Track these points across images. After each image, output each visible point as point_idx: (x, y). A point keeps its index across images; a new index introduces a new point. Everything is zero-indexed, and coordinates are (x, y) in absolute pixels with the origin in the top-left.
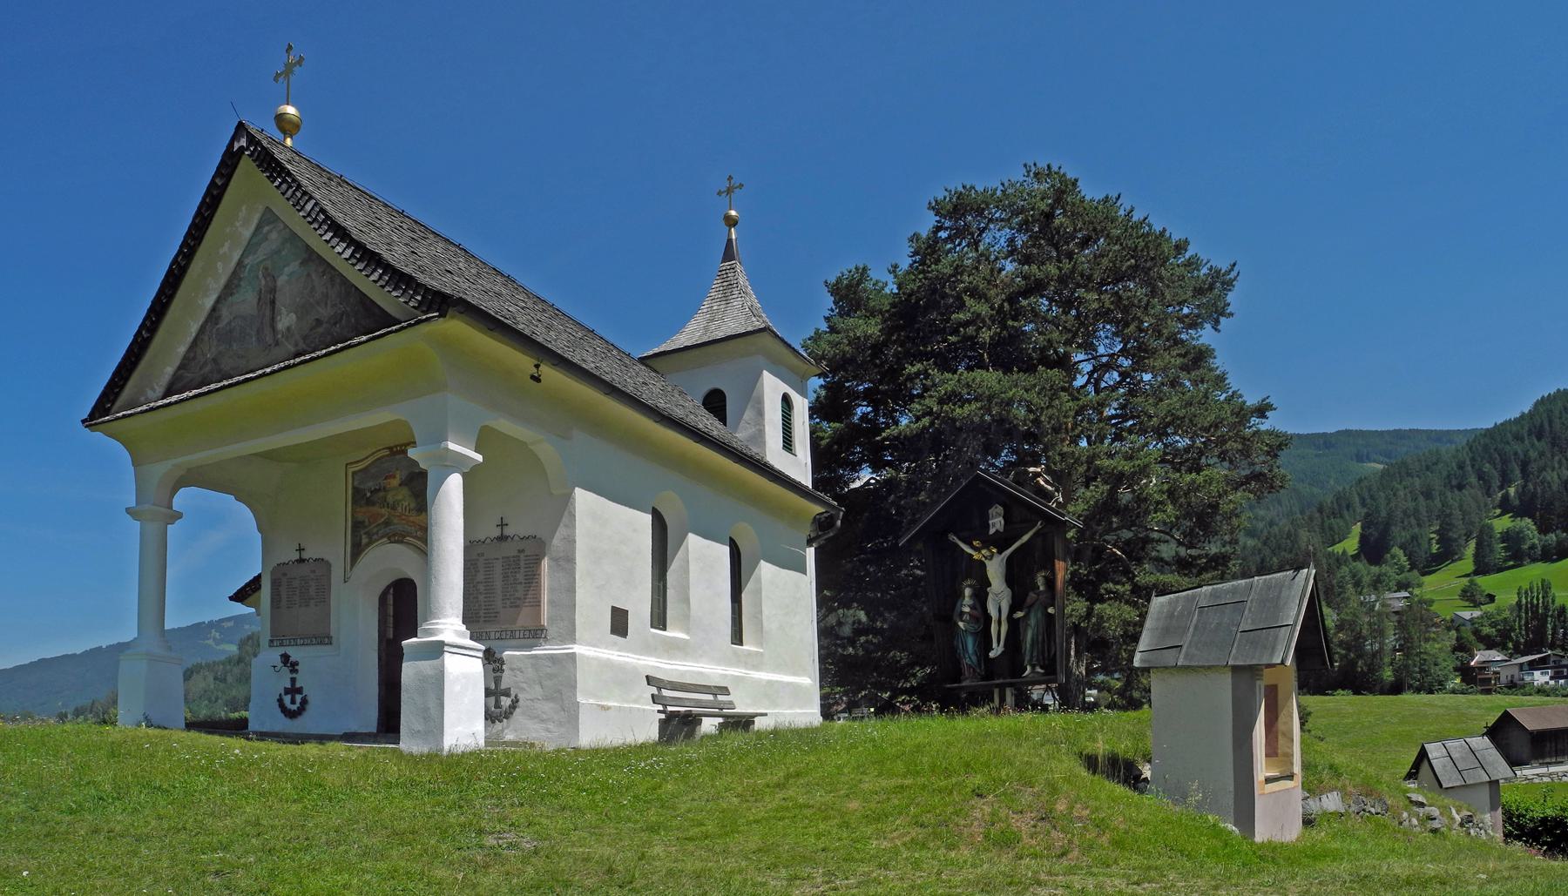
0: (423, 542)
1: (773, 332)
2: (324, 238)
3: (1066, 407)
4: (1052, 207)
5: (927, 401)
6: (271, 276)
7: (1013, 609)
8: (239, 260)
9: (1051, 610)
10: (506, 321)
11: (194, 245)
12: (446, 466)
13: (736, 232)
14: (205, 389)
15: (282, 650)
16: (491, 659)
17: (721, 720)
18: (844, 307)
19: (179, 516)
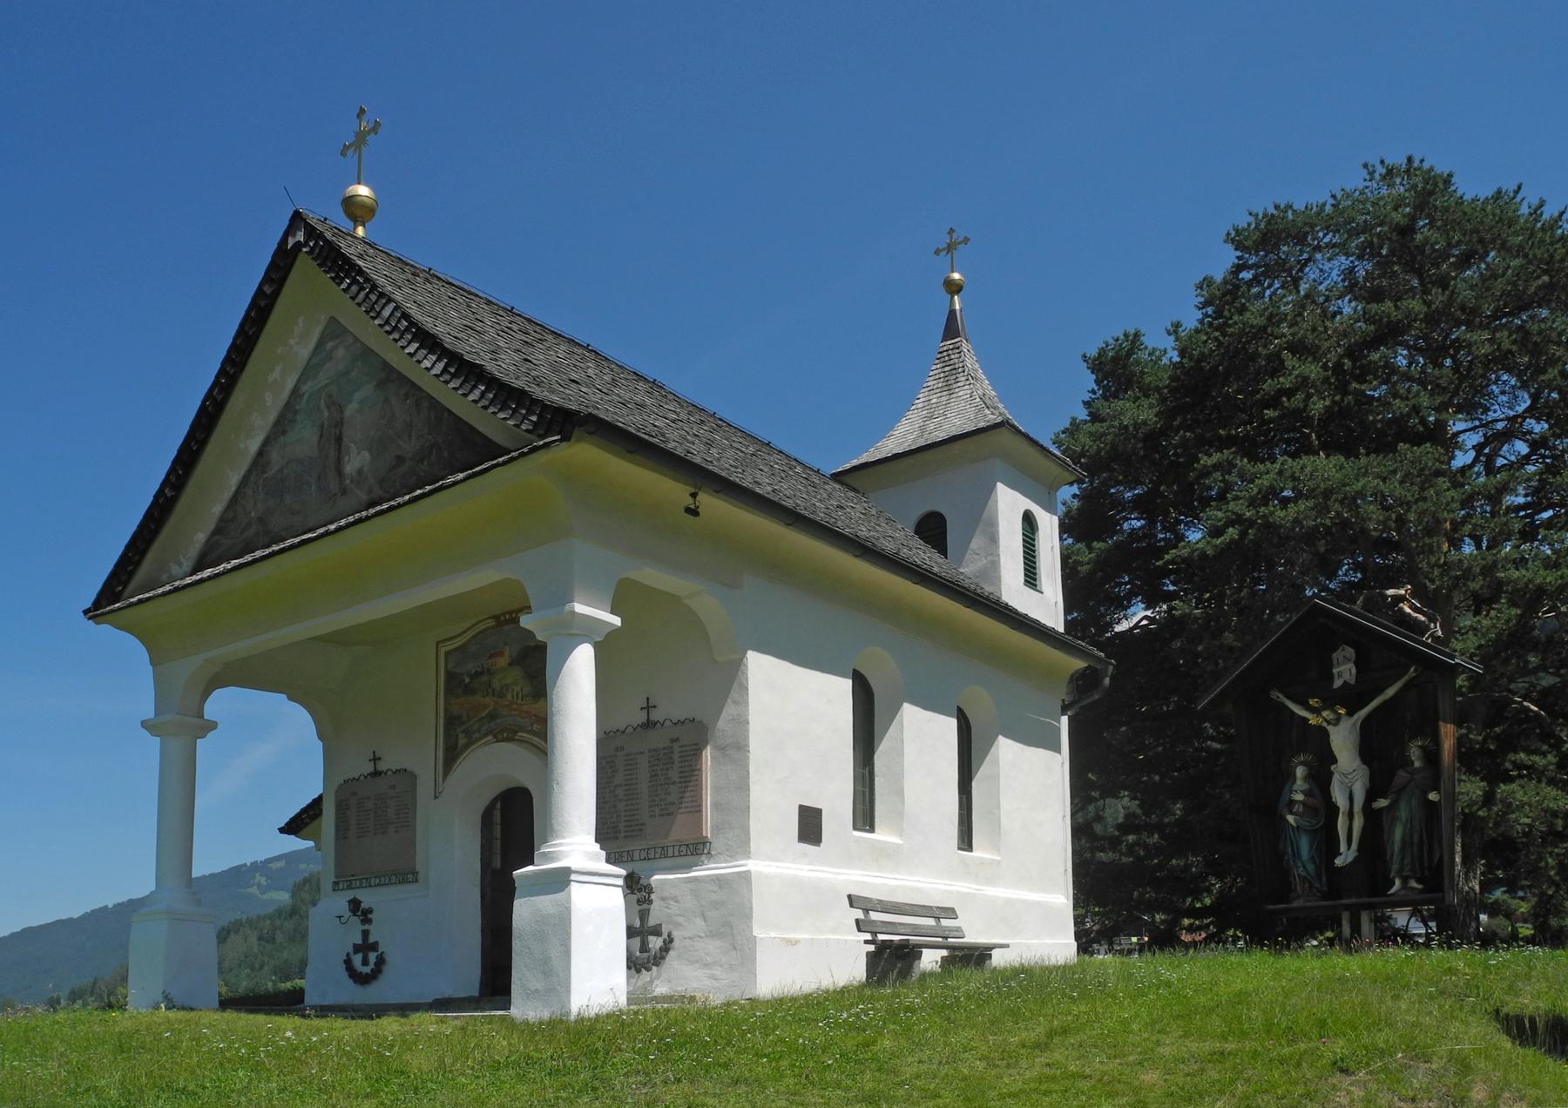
0: (540, 738)
1: (1013, 426)
2: (407, 351)
3: (1445, 497)
4: (1413, 219)
5: (1232, 505)
6: (337, 406)
7: (1371, 795)
8: (295, 386)
9: (1433, 796)
10: (651, 439)
11: (235, 373)
12: (572, 635)
13: (961, 301)
14: (248, 558)
15: (350, 895)
16: (635, 887)
17: (945, 953)
18: (1110, 387)
19: (212, 726)
